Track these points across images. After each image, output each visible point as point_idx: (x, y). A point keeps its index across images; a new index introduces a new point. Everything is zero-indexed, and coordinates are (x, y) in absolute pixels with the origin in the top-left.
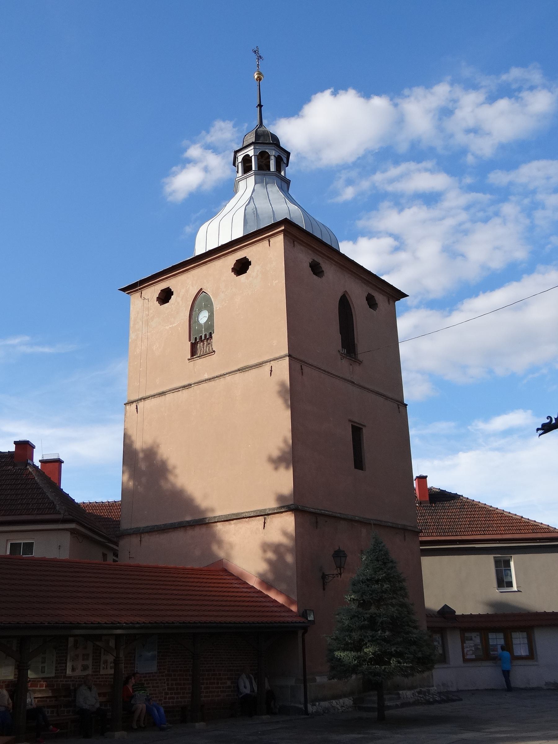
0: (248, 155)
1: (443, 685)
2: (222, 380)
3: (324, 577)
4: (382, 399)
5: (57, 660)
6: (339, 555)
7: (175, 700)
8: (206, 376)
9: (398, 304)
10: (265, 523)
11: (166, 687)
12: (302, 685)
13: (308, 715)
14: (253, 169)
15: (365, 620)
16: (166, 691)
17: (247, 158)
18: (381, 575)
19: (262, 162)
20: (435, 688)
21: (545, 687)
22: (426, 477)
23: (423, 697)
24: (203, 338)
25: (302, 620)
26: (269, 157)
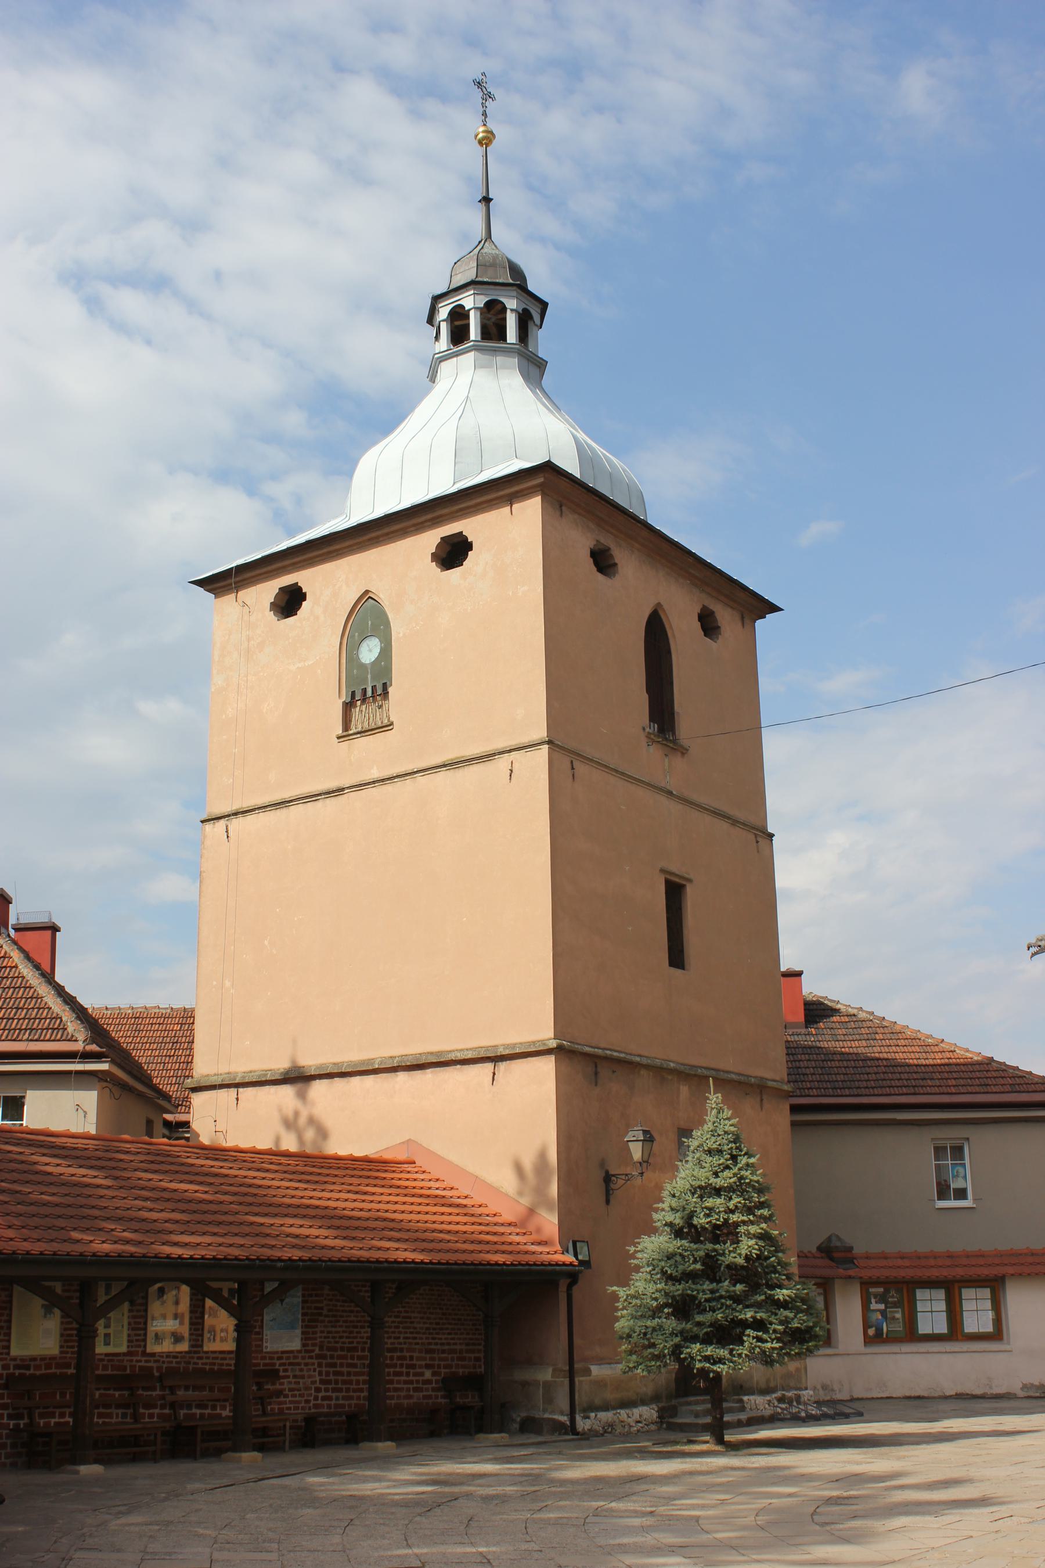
0: (462, 307)
1: (825, 1387)
4: (724, 826)
5: (129, 1324)
7: (333, 1402)
8: (375, 774)
10: (494, 1074)
11: (318, 1379)
12: (567, 1381)
13: (578, 1434)
14: (472, 337)
15: (695, 1261)
16: (318, 1385)
17: (458, 310)
18: (726, 1179)
19: (489, 319)
20: (811, 1393)
21: (1021, 1394)
23: (786, 1409)
24: (369, 693)
26: (504, 309)
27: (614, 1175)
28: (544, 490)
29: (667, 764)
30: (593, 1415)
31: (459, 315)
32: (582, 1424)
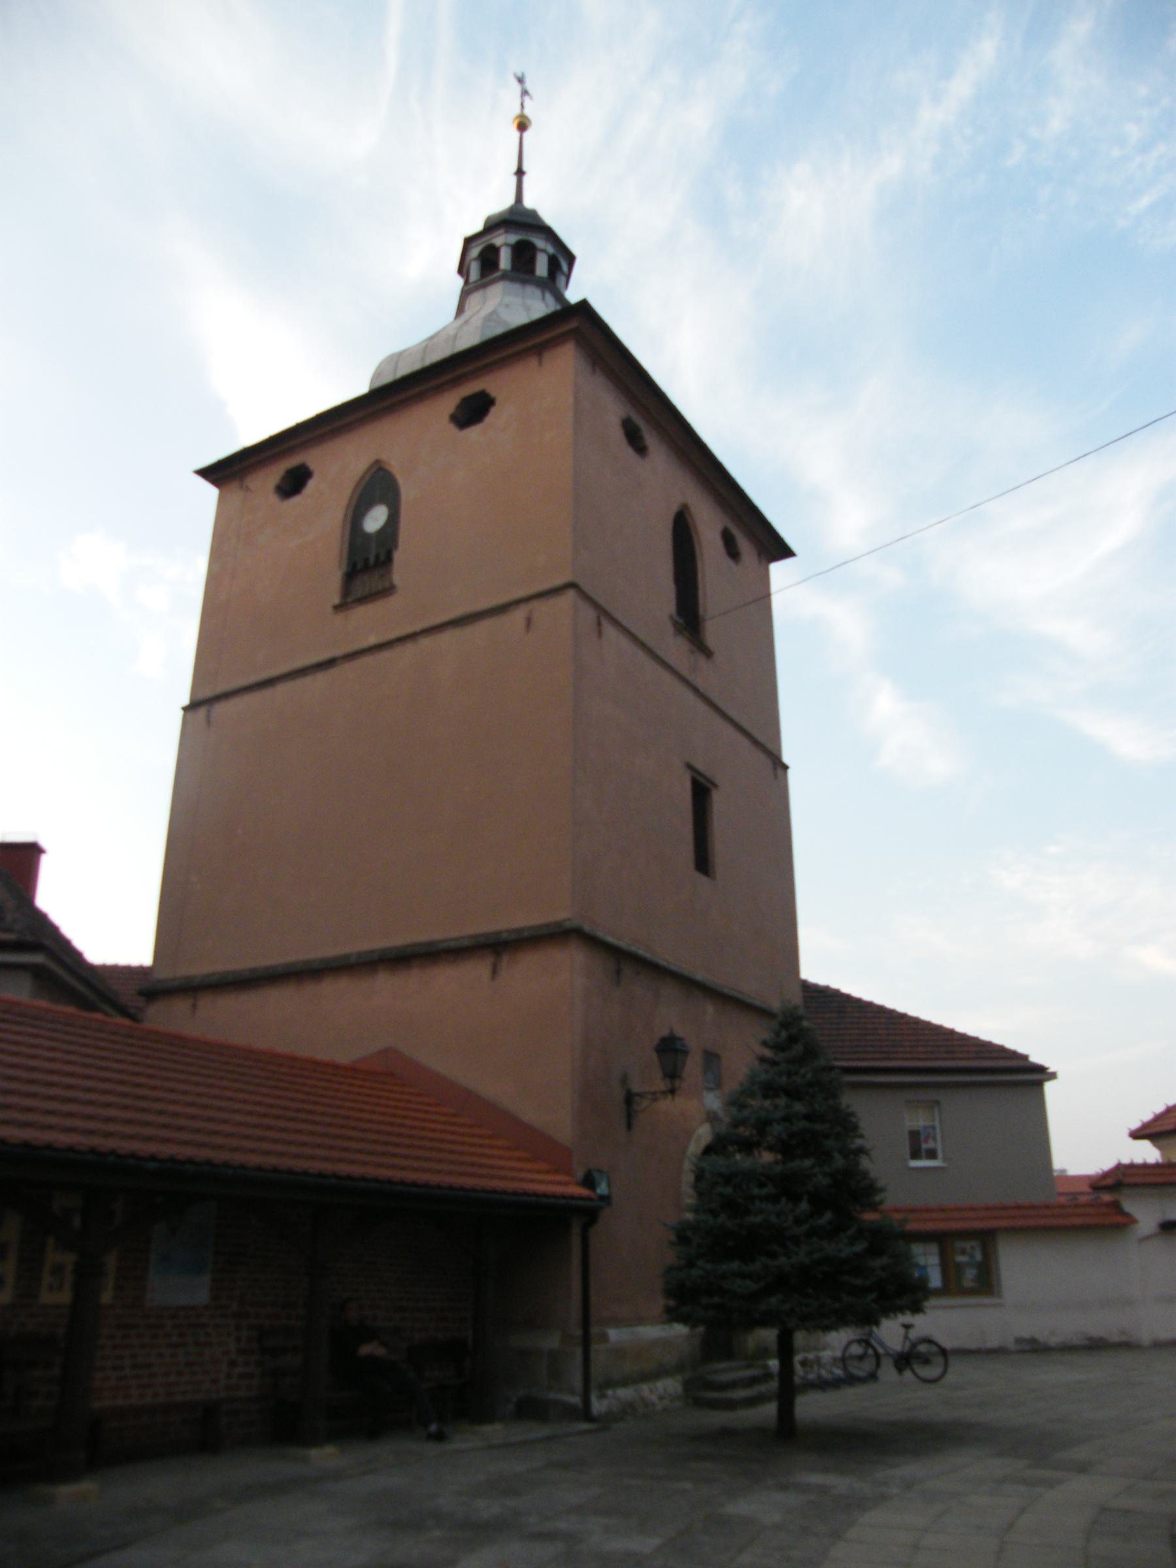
2: (410, 648)
3: (630, 1099)
8: (373, 640)
9: (778, 571)
12: (579, 1352)
25: (584, 1192)
27: (638, 1095)
30: (610, 1392)
32: (598, 1406)
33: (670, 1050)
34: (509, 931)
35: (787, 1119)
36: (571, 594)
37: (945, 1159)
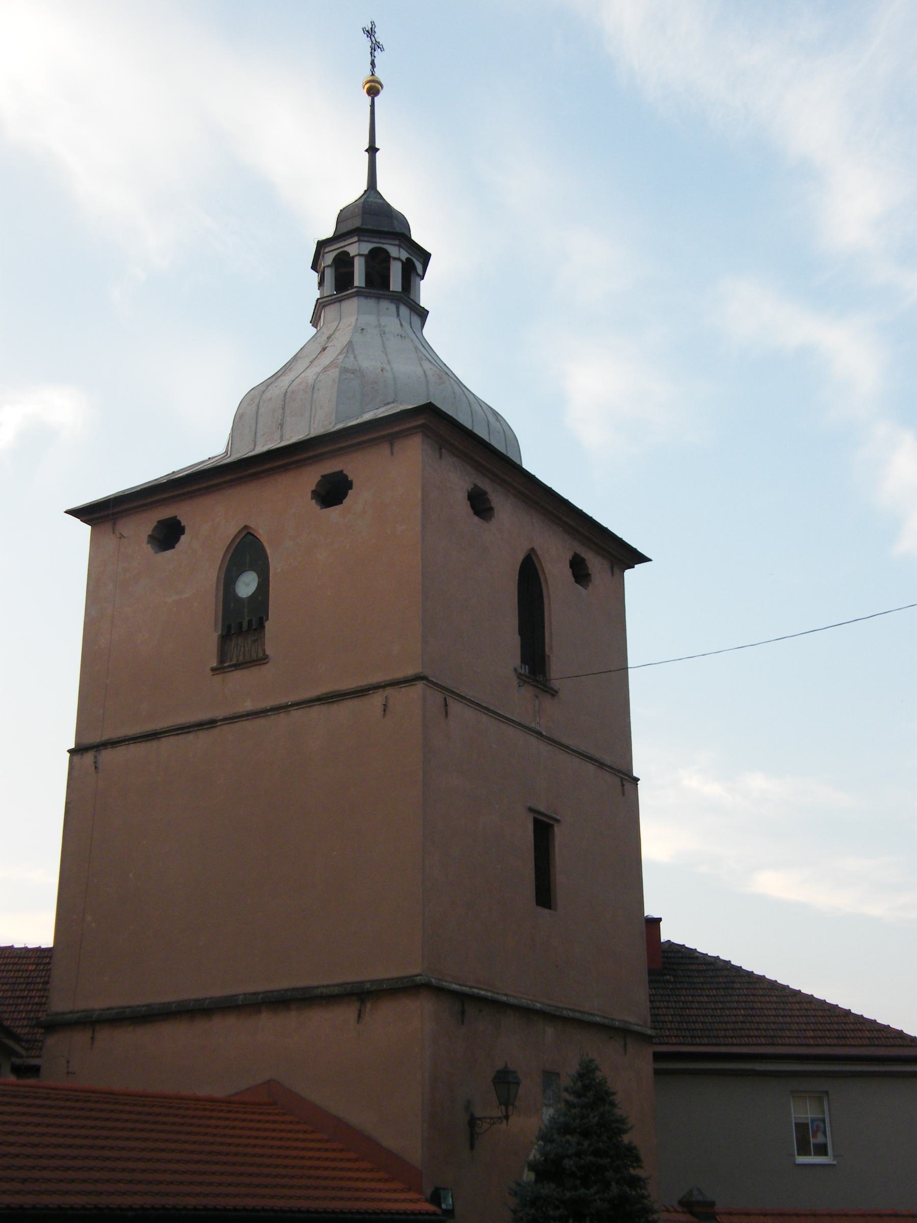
0: (346, 254)
2: (282, 720)
3: (472, 1122)
4: (591, 768)
6: (505, 1082)
8: (249, 706)
9: (632, 576)
14: (356, 283)
22: (660, 920)
24: (245, 625)
25: (432, 1208)
27: (479, 1119)
28: (425, 430)
29: (537, 704)
31: (343, 264)
33: (505, 1082)
34: (373, 982)
35: (578, 1154)
36: (420, 685)
37: (835, 1157)
